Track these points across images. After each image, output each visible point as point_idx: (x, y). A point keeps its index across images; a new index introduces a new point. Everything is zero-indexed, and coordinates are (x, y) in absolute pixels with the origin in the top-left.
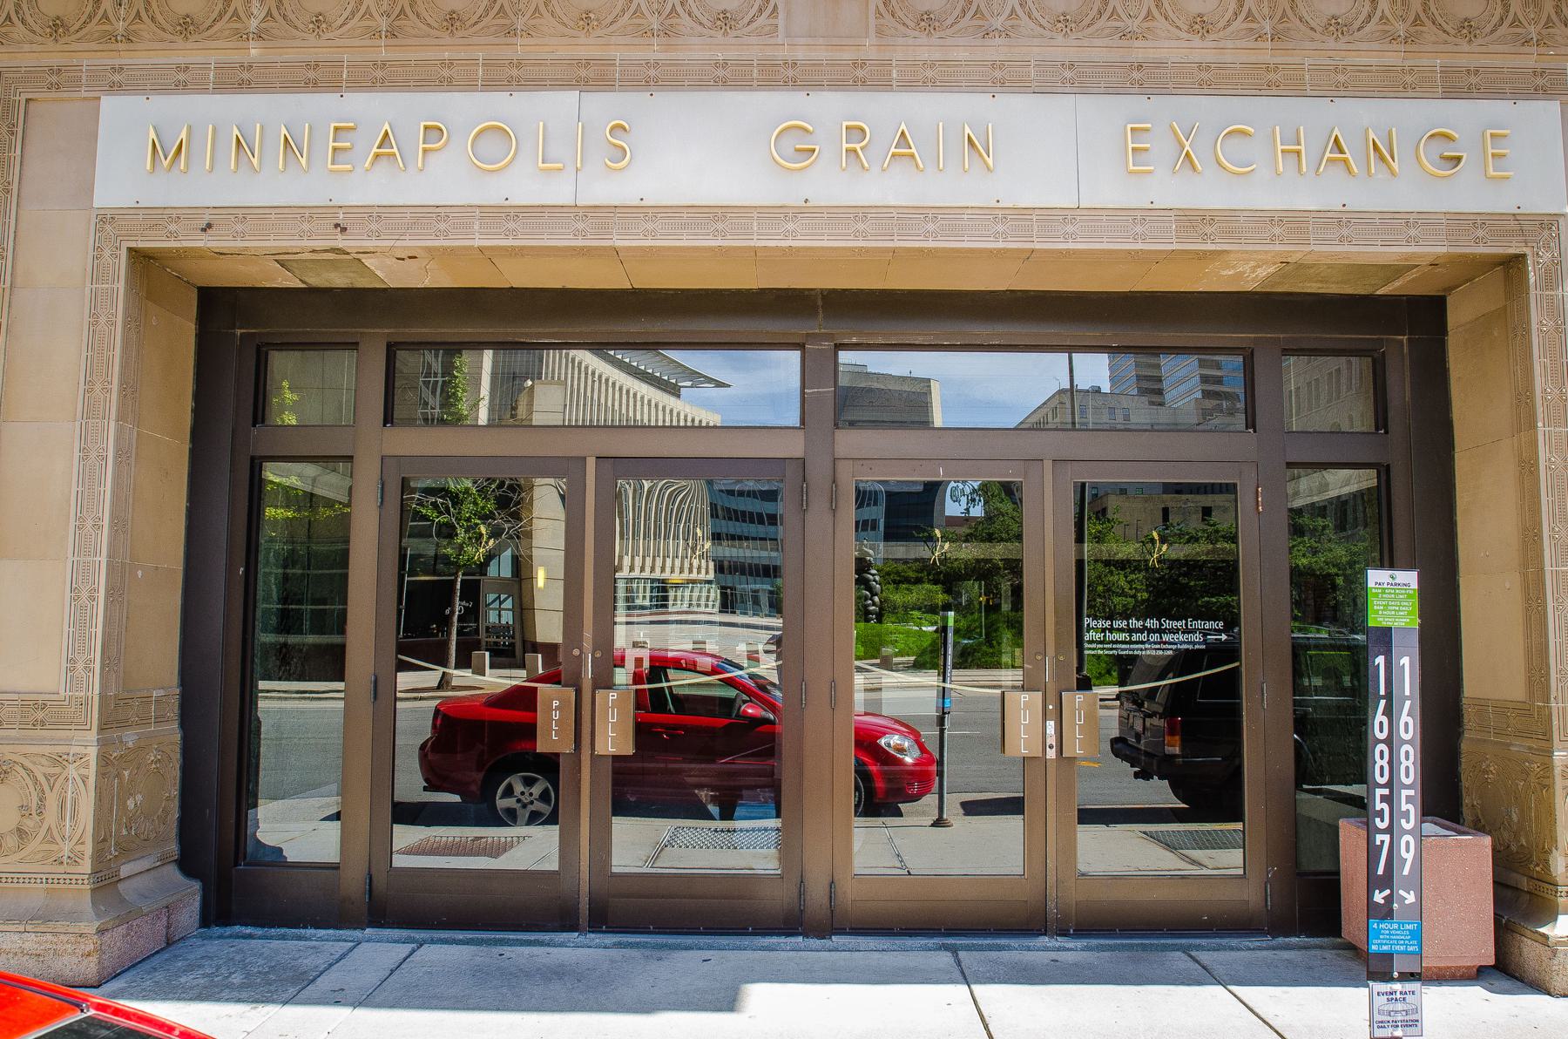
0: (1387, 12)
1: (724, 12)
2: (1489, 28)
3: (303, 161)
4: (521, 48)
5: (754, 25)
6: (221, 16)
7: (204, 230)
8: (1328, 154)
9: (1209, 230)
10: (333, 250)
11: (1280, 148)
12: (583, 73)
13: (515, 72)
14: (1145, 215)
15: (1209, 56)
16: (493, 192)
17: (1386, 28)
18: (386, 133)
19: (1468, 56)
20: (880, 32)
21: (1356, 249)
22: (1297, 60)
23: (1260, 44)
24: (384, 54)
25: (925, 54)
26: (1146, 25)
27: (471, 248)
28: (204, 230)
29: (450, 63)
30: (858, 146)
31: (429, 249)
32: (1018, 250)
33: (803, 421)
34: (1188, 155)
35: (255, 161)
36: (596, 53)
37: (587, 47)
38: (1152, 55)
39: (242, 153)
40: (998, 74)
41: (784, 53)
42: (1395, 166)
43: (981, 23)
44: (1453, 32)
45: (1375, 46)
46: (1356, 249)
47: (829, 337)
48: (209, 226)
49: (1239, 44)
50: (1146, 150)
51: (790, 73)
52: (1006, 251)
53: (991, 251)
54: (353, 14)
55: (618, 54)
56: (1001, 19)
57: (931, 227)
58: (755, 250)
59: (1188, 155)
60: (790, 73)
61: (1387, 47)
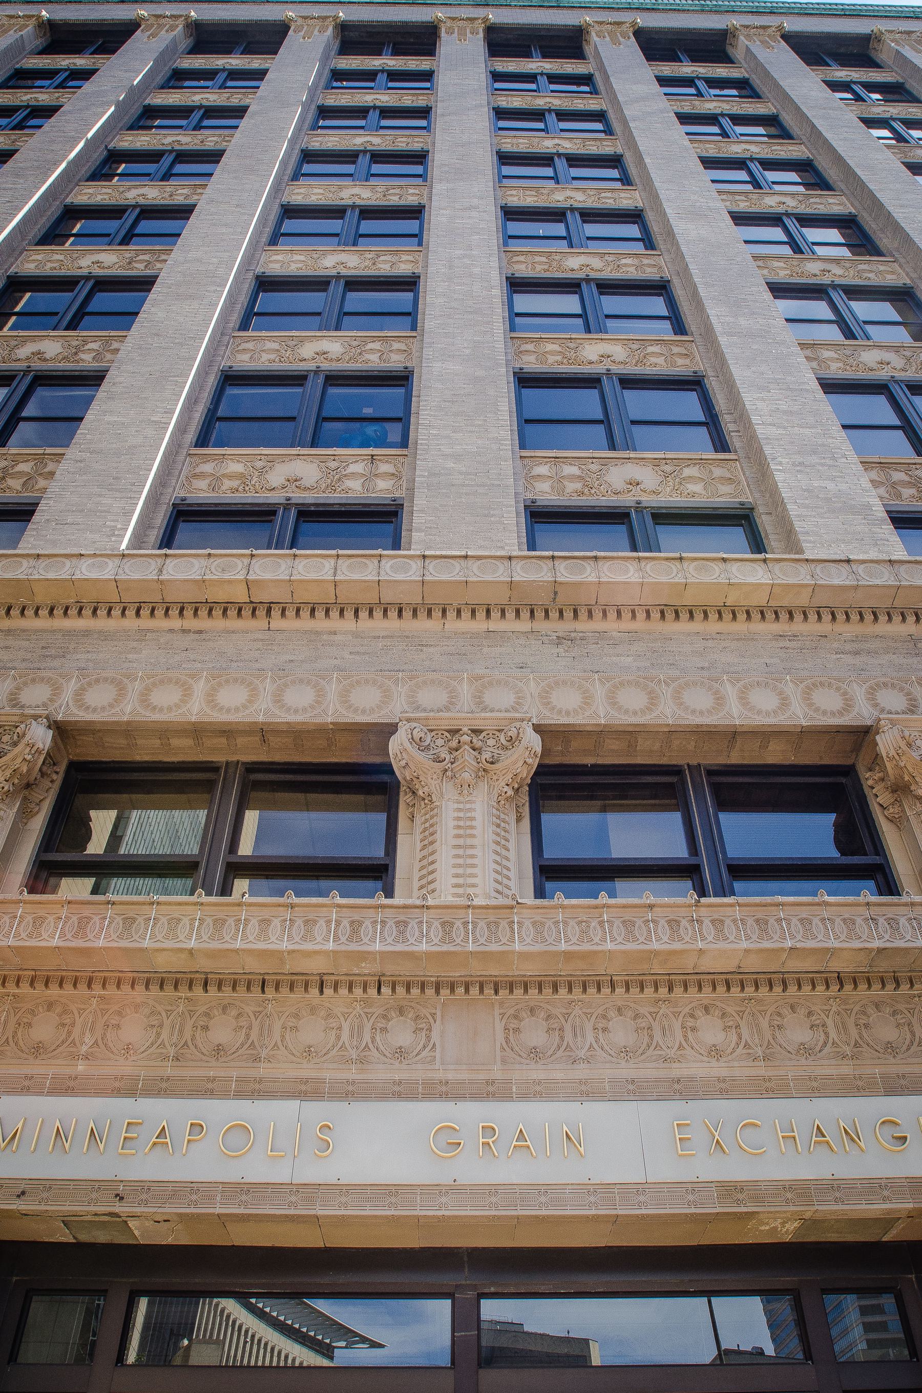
0: (836, 1039)
1: (400, 1048)
2: (905, 1047)
3: (102, 1146)
4: (263, 1070)
5: (420, 1057)
6: (63, 1042)
7: (19, 1196)
8: (814, 1138)
9: (740, 1196)
10: (111, 1214)
11: (780, 1135)
12: (304, 1088)
13: (257, 1086)
14: (694, 1187)
15: (724, 1073)
16: (233, 1172)
17: (837, 1050)
18: (164, 1127)
19: (894, 1067)
20: (504, 1061)
21: (848, 1207)
22: (782, 1073)
23: (756, 1063)
24: (169, 1072)
25: (534, 1075)
26: (679, 1053)
27: (213, 1214)
28: (19, 1196)
29: (213, 1080)
30: (490, 1141)
31: (180, 1215)
32: (606, 1216)
33: (453, 1362)
34: (717, 1141)
35: (67, 1145)
36: (313, 1074)
37: (307, 1071)
38: (686, 1072)
39: (59, 1137)
40: (583, 1088)
41: (440, 1075)
42: (862, 1144)
43: (570, 1054)
44: (882, 1051)
45: (833, 1062)
46: (848, 1207)
47: (474, 1287)
48: (23, 1193)
49: (742, 1063)
50: (689, 1139)
51: (444, 1089)
52: (598, 1216)
53: (587, 1217)
54: (152, 1044)
55: (327, 1075)
56: (583, 1051)
57: (543, 1199)
58: (418, 1218)
59: (717, 1141)
60: (444, 1089)
61: (840, 1062)
